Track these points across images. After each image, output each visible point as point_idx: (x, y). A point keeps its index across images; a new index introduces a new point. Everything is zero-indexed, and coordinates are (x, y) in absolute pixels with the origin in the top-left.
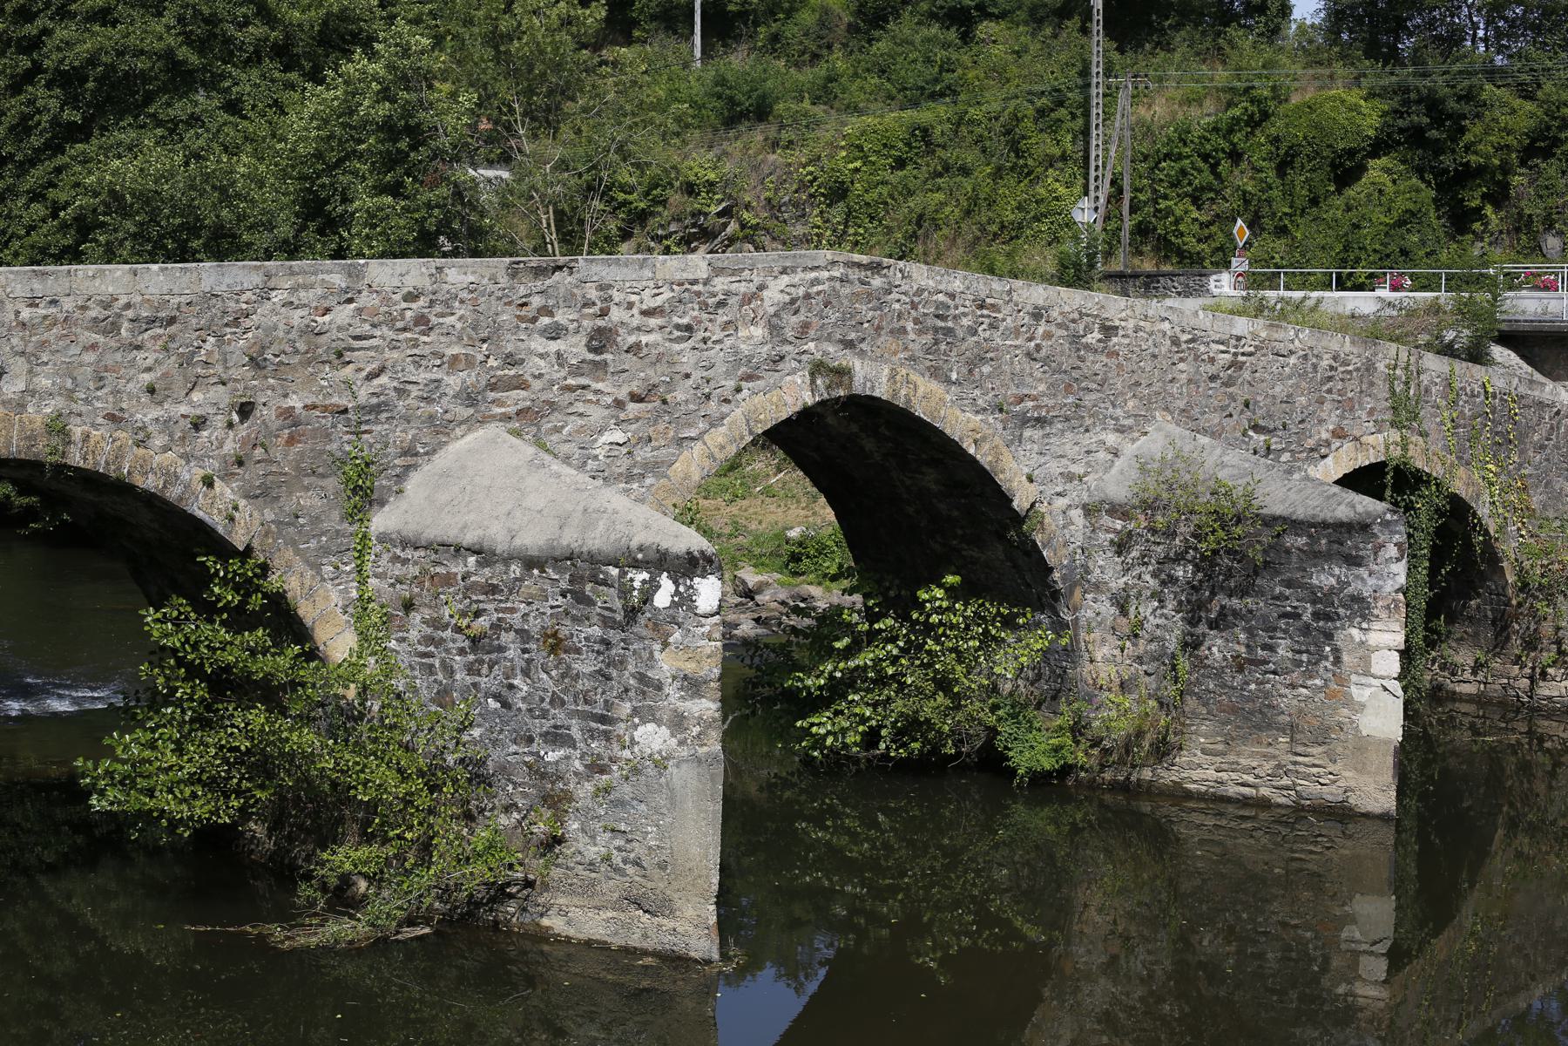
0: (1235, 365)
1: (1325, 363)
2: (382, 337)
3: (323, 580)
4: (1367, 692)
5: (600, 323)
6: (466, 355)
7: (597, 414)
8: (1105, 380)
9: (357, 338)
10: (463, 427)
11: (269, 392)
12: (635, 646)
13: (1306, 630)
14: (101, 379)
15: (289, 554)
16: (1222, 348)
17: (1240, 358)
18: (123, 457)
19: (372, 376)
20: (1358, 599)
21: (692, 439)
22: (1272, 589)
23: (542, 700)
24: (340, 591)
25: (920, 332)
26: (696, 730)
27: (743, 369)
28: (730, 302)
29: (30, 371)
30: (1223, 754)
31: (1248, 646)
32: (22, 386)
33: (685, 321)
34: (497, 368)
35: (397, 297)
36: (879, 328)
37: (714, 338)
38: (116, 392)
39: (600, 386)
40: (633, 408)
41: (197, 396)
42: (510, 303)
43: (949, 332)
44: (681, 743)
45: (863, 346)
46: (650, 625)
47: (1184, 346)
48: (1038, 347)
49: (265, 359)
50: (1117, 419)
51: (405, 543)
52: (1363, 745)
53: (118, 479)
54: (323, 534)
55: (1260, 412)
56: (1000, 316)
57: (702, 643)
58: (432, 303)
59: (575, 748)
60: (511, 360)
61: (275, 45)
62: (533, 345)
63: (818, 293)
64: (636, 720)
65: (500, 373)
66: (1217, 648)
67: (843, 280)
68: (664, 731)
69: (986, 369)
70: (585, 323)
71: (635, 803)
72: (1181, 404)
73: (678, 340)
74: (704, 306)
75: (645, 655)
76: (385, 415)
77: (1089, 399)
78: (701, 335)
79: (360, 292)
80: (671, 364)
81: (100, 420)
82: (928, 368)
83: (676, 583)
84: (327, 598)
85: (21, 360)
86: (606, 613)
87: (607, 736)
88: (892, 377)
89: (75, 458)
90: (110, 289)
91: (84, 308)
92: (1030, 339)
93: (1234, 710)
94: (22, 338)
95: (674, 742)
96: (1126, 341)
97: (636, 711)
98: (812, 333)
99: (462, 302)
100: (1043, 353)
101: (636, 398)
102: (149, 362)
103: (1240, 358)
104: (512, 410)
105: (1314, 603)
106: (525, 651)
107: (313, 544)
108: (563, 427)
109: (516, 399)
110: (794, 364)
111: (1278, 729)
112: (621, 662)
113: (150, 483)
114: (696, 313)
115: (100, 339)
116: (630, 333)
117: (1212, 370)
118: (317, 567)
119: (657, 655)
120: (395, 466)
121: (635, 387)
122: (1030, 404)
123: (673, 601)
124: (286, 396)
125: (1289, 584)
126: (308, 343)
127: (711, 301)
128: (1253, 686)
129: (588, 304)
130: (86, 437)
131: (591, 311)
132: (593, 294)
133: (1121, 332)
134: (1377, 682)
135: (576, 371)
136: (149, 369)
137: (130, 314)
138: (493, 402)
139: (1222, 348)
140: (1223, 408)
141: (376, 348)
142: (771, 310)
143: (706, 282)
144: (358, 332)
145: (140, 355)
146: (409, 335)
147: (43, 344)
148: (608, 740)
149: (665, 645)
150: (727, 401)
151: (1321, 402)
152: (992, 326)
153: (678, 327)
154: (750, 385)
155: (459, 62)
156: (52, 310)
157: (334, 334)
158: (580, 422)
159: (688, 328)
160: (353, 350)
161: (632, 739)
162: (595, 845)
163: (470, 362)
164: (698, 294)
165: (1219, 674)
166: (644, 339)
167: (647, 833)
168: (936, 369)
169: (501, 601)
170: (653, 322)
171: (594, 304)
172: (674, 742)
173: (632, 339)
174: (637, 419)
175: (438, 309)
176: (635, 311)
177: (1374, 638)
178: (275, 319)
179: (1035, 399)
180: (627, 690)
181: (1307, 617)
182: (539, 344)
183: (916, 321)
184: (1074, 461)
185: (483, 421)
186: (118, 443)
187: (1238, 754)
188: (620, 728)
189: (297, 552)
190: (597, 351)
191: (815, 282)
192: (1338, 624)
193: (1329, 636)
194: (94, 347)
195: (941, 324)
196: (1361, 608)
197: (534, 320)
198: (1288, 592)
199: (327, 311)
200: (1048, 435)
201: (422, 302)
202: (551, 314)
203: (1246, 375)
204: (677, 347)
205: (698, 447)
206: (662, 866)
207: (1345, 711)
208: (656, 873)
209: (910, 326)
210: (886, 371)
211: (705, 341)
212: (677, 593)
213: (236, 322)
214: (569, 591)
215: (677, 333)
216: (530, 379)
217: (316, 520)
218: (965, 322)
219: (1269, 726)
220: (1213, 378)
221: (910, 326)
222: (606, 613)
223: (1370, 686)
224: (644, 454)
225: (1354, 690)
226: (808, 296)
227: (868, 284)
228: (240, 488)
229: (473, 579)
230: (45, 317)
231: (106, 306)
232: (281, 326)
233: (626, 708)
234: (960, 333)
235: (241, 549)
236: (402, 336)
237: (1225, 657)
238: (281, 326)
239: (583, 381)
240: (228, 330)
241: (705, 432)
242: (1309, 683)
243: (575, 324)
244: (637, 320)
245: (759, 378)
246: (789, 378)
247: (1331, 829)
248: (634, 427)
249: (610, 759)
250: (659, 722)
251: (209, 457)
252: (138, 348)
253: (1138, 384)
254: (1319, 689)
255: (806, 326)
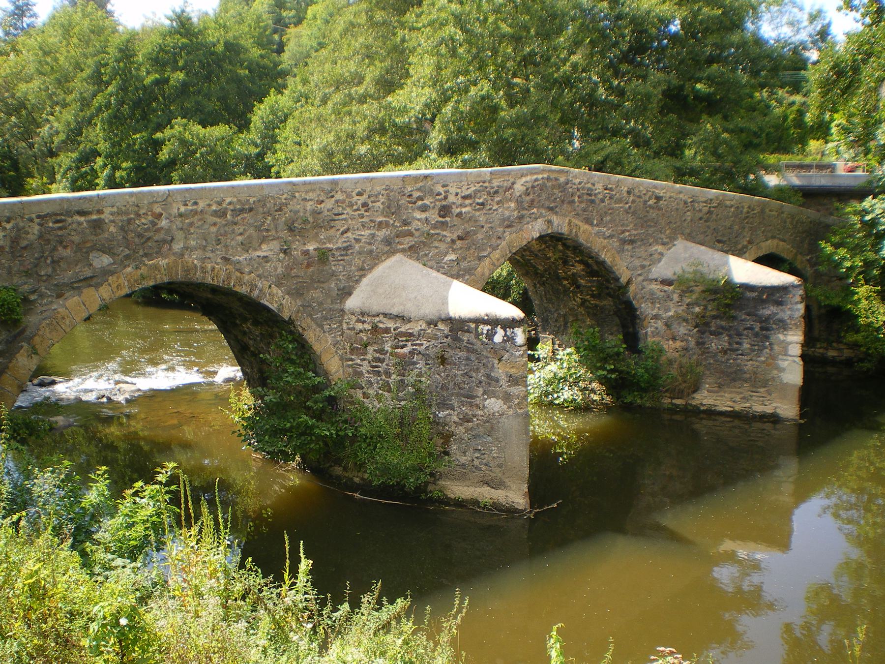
0: (710, 212)
1: (745, 210)
2: (347, 214)
3: (324, 332)
4: (786, 363)
5: (444, 203)
6: (386, 221)
7: (443, 246)
8: (657, 221)
9: (336, 215)
10: (385, 255)
11: (297, 243)
12: (484, 361)
13: (756, 335)
14: (219, 240)
15: (309, 320)
16: (705, 204)
17: (712, 209)
18: (231, 278)
19: (343, 233)
20: (781, 321)
21: (485, 257)
22: (741, 316)
23: (437, 387)
24: (332, 337)
25: (580, 202)
26: (516, 401)
27: (506, 223)
28: (500, 191)
29: (186, 238)
30: (717, 392)
31: (729, 343)
32: (182, 245)
33: (481, 201)
34: (400, 226)
35: (354, 194)
36: (563, 202)
37: (494, 208)
38: (226, 246)
39: (445, 233)
40: (459, 243)
41: (264, 247)
42: (404, 195)
43: (592, 202)
44: (509, 407)
45: (557, 209)
46: (492, 351)
47: (689, 204)
48: (630, 207)
49: (295, 227)
50: (662, 239)
51: (363, 314)
52: (785, 386)
53: (228, 289)
54: (324, 310)
55: (720, 234)
56: (614, 193)
57: (519, 359)
58: (369, 196)
59: (454, 410)
60: (406, 223)
61: (541, 17)
62: (415, 215)
63: (538, 185)
64: (486, 397)
65: (400, 229)
66: (715, 344)
67: (548, 179)
68: (500, 402)
69: (608, 218)
70: (437, 203)
71: (485, 436)
72: (688, 231)
73: (479, 210)
74: (489, 193)
75: (490, 365)
76: (350, 251)
77: (651, 231)
78: (488, 207)
79: (337, 192)
80: (476, 221)
81: (219, 260)
82: (584, 219)
83: (505, 331)
84: (327, 341)
85: (181, 232)
86: (469, 346)
87: (471, 405)
88: (569, 223)
89: (209, 280)
90: (222, 195)
91: (209, 205)
92: (627, 203)
93: (722, 372)
94: (181, 222)
95: (505, 407)
96: (666, 203)
97: (485, 393)
98: (535, 203)
99: (383, 195)
100: (632, 209)
101: (460, 238)
102: (241, 230)
103: (712, 209)
104: (406, 246)
105: (761, 322)
106: (427, 364)
107: (319, 315)
108: (429, 253)
109: (408, 242)
110: (528, 219)
111: (743, 380)
112: (477, 369)
113: (243, 290)
114: (485, 197)
115: (218, 220)
116: (457, 207)
117: (700, 215)
118: (322, 327)
119: (496, 365)
120: (355, 276)
121: (460, 233)
122: (627, 234)
123: (503, 339)
124: (305, 244)
125: (748, 314)
126: (314, 218)
127: (492, 191)
128: (731, 361)
129: (439, 194)
130: (213, 269)
131: (440, 197)
132: (441, 190)
133: (664, 199)
134: (790, 358)
135: (435, 227)
136: (241, 234)
137: (231, 207)
138: (398, 243)
139: (705, 204)
140: (705, 232)
141: (345, 219)
142: (518, 194)
143: (490, 182)
144: (336, 212)
145: (236, 228)
146: (360, 212)
147: (191, 224)
148: (471, 406)
149: (500, 360)
150: (499, 238)
151: (744, 228)
152: (611, 198)
153: (478, 204)
154: (510, 229)
155: (316, 86)
156: (195, 207)
157: (326, 213)
158: (436, 251)
159: (482, 204)
160: (334, 220)
161: (484, 406)
162: (465, 456)
163: (387, 224)
164: (486, 188)
165: (715, 355)
166: (464, 210)
167: (492, 450)
168: (588, 219)
169: (414, 340)
170: (467, 202)
171: (441, 194)
172: (505, 407)
173: (458, 210)
174: (461, 248)
175: (372, 199)
176: (459, 196)
177: (790, 338)
178: (299, 207)
179: (628, 231)
180: (480, 382)
181: (757, 329)
182: (418, 215)
183: (579, 197)
184: (645, 259)
185: (394, 253)
186: (228, 271)
187: (725, 392)
188: (478, 401)
189: (313, 319)
190: (443, 217)
191: (536, 180)
192: (772, 332)
193: (767, 338)
194: (215, 224)
195: (590, 198)
196: (783, 326)
197: (415, 203)
198: (748, 318)
199: (322, 201)
200: (634, 248)
201: (365, 196)
202: (422, 200)
203: (714, 216)
204: (478, 213)
205: (488, 260)
206: (500, 466)
207: (775, 372)
208: (498, 470)
209: (576, 199)
210: (567, 221)
211: (490, 209)
212: (506, 335)
213: (280, 210)
214: (449, 335)
215: (478, 207)
216: (414, 231)
217: (320, 304)
218: (600, 196)
219: (740, 379)
220: (701, 219)
221: (576, 199)
222: (469, 346)
223: (787, 360)
224: (464, 265)
225: (780, 362)
226: (533, 187)
227: (558, 180)
228: (285, 290)
229: (399, 330)
230: (192, 210)
231: (220, 204)
232: (301, 210)
233: (480, 391)
234: (597, 202)
235: (287, 319)
236: (356, 213)
237: (718, 348)
238: (301, 210)
239: (437, 231)
240: (277, 213)
241: (491, 253)
242: (759, 359)
243: (433, 204)
244: (460, 201)
245: (513, 226)
246: (526, 226)
247: (768, 426)
248: (460, 252)
249: (473, 415)
250: (497, 398)
251: (271, 276)
252: (236, 224)
253: (670, 222)
254: (763, 362)
255: (532, 201)
